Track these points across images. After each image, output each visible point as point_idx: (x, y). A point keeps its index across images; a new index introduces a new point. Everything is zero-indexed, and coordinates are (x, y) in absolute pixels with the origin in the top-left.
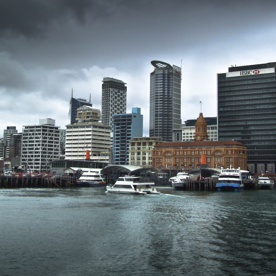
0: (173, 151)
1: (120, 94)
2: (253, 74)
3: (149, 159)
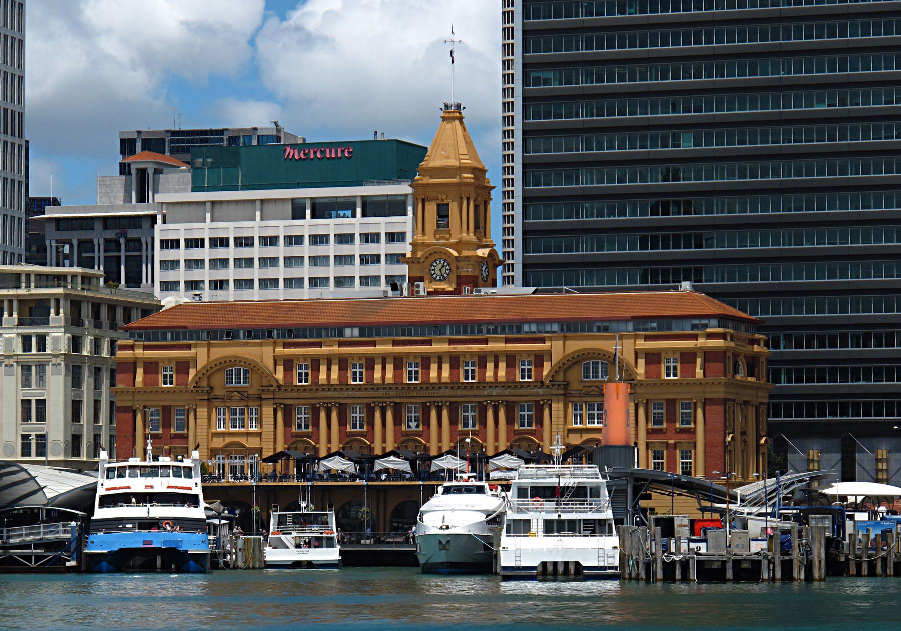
0: (270, 364)
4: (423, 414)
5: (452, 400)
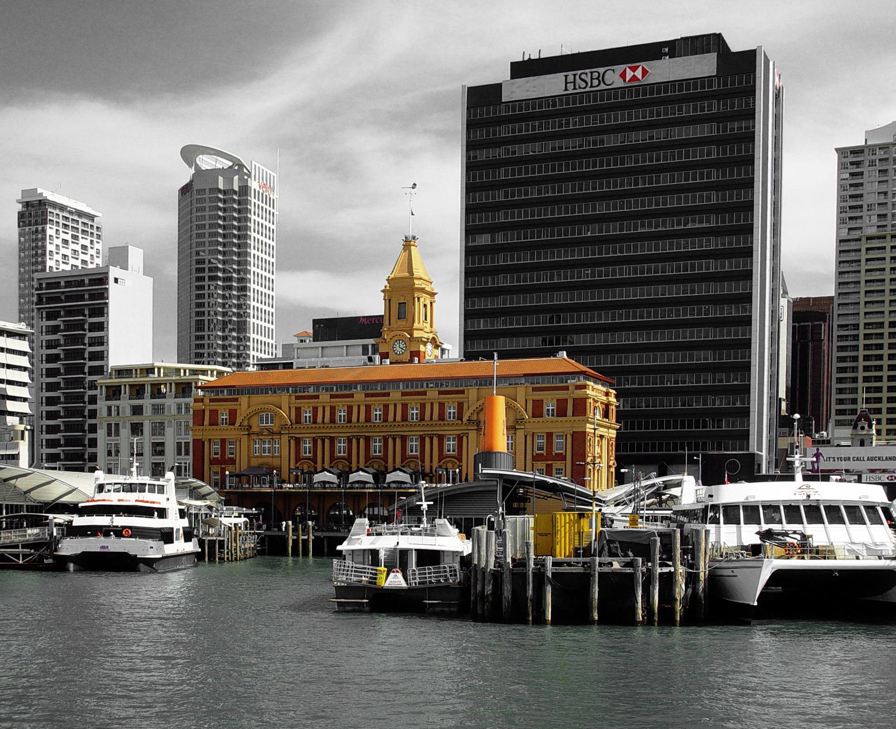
1: (78, 248)
2: (619, 83)
3: (179, 453)
4: (458, 443)
5: (402, 434)
